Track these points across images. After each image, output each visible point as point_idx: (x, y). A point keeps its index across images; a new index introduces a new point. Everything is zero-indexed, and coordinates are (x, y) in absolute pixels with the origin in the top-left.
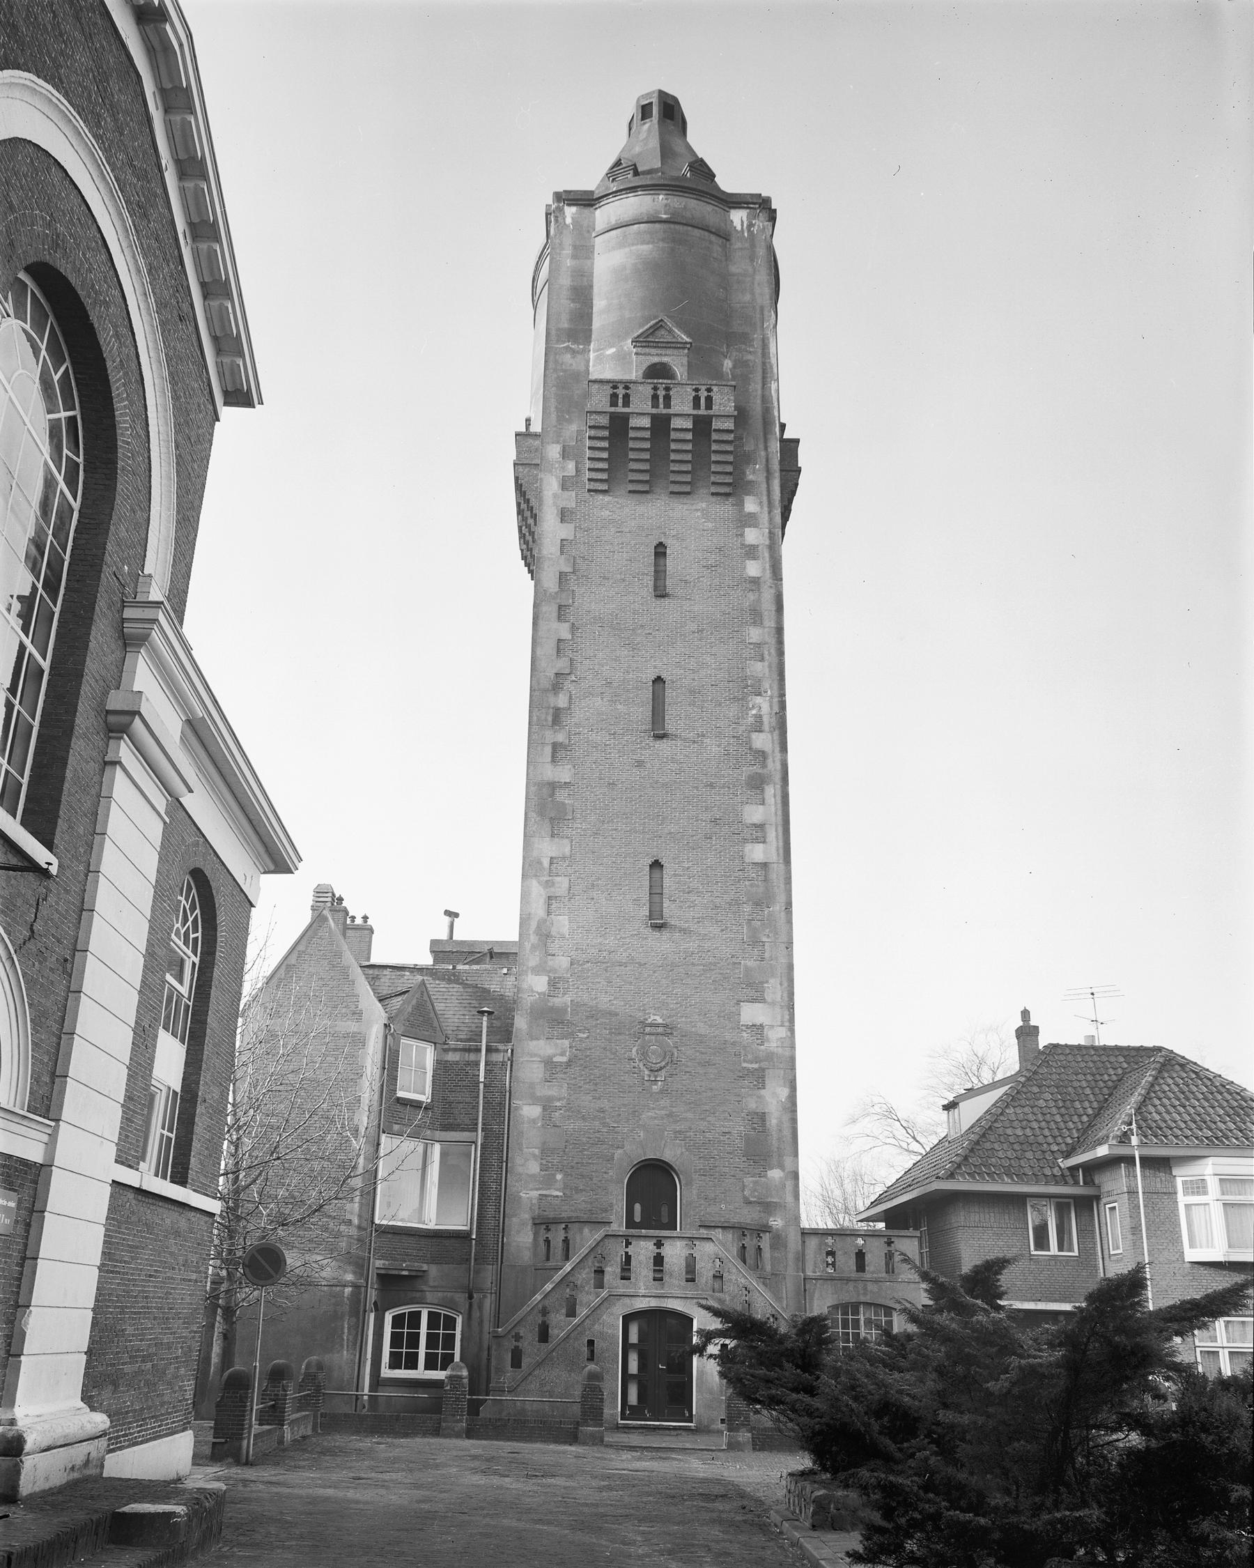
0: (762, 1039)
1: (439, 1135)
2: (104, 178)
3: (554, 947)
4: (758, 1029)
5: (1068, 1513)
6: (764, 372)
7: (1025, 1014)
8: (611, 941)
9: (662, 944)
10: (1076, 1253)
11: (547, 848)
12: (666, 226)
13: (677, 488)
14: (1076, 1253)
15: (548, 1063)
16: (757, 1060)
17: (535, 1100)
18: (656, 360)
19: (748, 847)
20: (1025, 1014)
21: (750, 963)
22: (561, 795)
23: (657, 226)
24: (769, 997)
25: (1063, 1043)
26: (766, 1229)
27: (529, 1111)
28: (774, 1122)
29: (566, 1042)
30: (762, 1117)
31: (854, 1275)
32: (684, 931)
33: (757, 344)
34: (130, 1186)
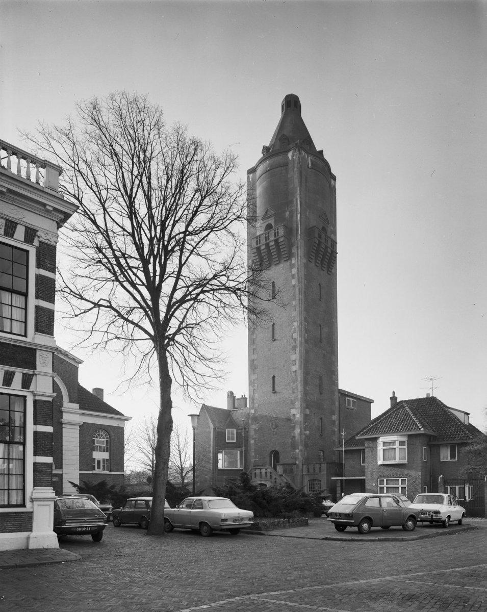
0: (295, 418)
1: (238, 449)
2: (161, 213)
3: (255, 401)
4: (294, 415)
5: (475, 588)
6: (296, 212)
7: (394, 392)
8: (266, 398)
9: (275, 397)
10: (235, 441)
11: (253, 377)
12: (270, 171)
13: (276, 263)
14: (227, 441)
15: (255, 430)
16: (293, 423)
17: (253, 439)
18: (267, 223)
19: (292, 367)
20: (394, 392)
21: (292, 398)
22: (255, 362)
23: (267, 173)
24: (296, 407)
25: (404, 400)
26: (295, 464)
27: (252, 442)
28: (297, 438)
29: (258, 425)
30: (294, 437)
31: (319, 473)
32: (279, 393)
33: (295, 202)
34: (196, 415)
